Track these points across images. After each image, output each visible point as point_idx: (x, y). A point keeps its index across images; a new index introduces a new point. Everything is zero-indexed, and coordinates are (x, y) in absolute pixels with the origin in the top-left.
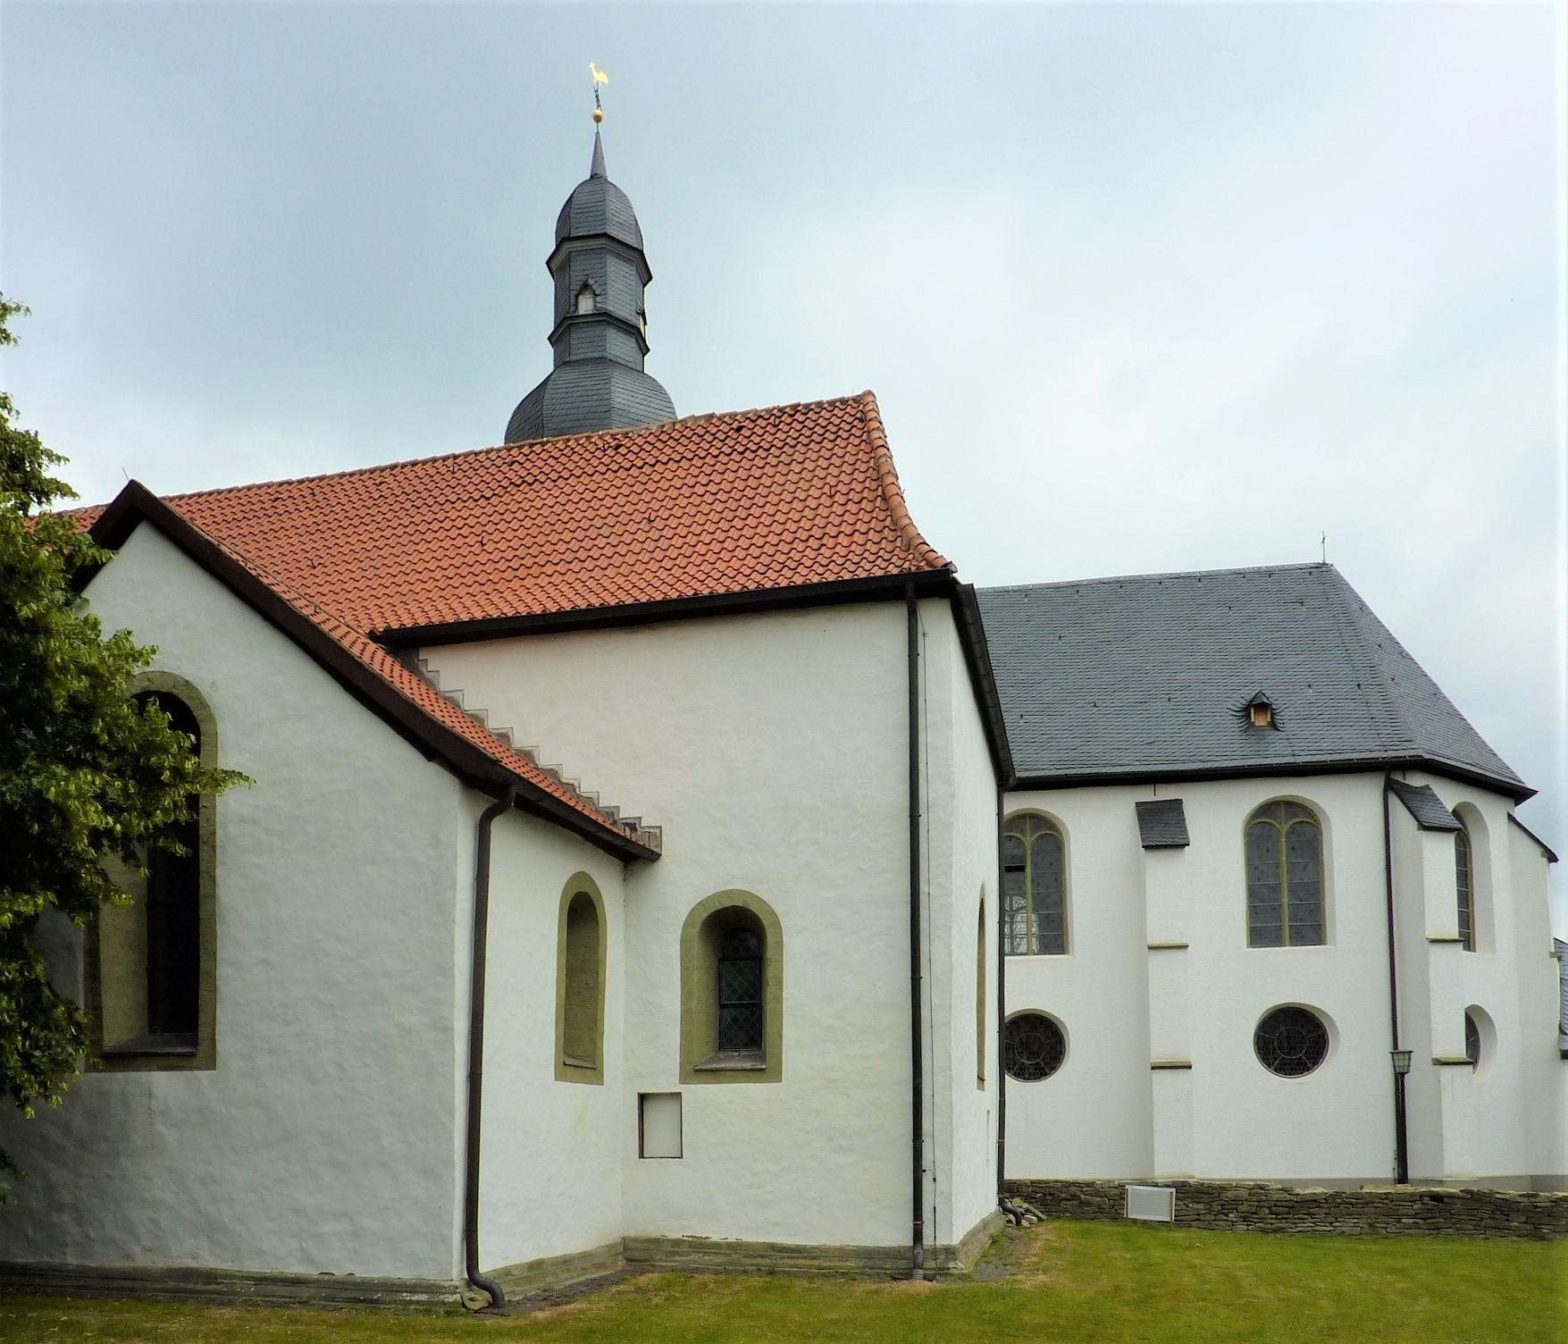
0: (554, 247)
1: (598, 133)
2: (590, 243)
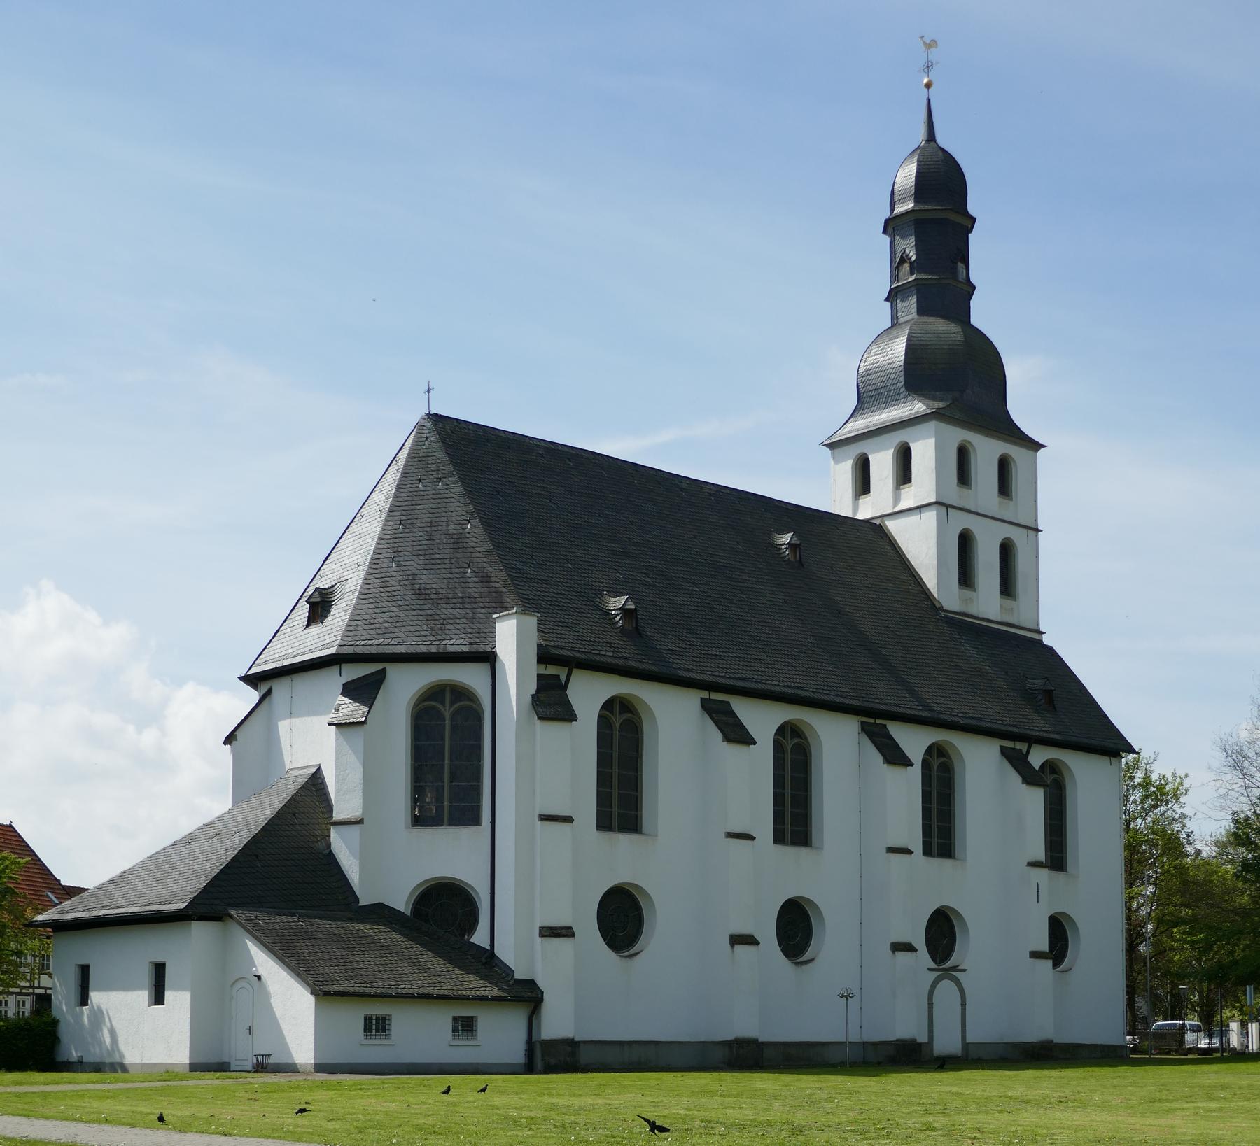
1: (929, 100)
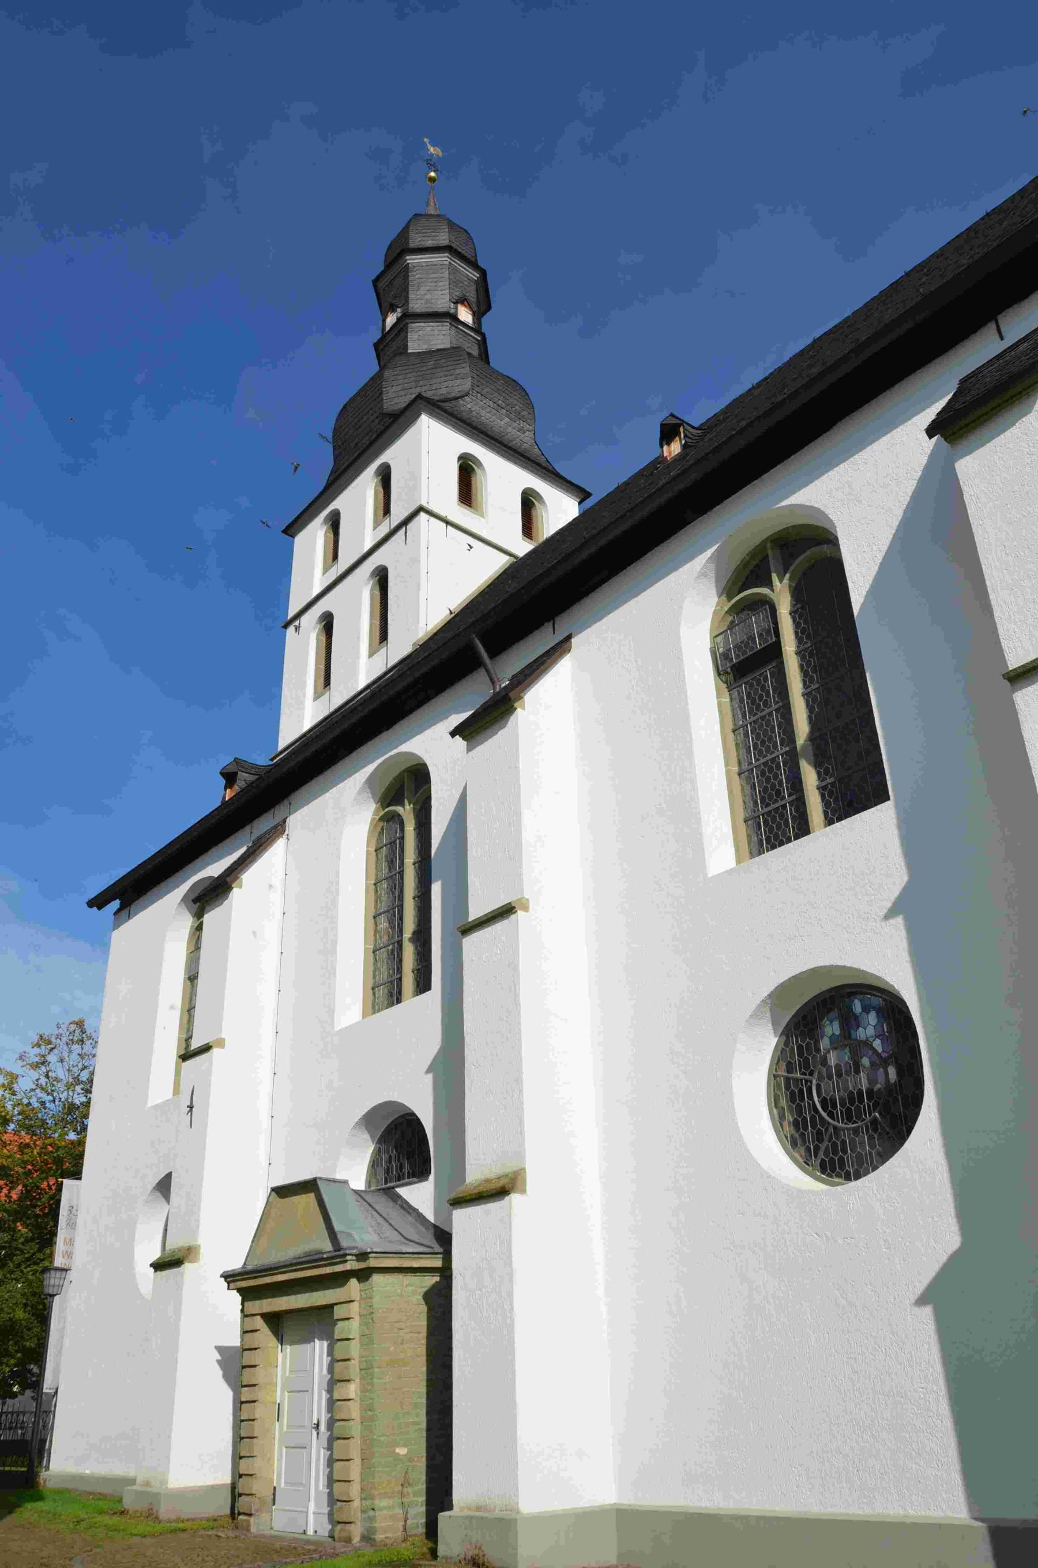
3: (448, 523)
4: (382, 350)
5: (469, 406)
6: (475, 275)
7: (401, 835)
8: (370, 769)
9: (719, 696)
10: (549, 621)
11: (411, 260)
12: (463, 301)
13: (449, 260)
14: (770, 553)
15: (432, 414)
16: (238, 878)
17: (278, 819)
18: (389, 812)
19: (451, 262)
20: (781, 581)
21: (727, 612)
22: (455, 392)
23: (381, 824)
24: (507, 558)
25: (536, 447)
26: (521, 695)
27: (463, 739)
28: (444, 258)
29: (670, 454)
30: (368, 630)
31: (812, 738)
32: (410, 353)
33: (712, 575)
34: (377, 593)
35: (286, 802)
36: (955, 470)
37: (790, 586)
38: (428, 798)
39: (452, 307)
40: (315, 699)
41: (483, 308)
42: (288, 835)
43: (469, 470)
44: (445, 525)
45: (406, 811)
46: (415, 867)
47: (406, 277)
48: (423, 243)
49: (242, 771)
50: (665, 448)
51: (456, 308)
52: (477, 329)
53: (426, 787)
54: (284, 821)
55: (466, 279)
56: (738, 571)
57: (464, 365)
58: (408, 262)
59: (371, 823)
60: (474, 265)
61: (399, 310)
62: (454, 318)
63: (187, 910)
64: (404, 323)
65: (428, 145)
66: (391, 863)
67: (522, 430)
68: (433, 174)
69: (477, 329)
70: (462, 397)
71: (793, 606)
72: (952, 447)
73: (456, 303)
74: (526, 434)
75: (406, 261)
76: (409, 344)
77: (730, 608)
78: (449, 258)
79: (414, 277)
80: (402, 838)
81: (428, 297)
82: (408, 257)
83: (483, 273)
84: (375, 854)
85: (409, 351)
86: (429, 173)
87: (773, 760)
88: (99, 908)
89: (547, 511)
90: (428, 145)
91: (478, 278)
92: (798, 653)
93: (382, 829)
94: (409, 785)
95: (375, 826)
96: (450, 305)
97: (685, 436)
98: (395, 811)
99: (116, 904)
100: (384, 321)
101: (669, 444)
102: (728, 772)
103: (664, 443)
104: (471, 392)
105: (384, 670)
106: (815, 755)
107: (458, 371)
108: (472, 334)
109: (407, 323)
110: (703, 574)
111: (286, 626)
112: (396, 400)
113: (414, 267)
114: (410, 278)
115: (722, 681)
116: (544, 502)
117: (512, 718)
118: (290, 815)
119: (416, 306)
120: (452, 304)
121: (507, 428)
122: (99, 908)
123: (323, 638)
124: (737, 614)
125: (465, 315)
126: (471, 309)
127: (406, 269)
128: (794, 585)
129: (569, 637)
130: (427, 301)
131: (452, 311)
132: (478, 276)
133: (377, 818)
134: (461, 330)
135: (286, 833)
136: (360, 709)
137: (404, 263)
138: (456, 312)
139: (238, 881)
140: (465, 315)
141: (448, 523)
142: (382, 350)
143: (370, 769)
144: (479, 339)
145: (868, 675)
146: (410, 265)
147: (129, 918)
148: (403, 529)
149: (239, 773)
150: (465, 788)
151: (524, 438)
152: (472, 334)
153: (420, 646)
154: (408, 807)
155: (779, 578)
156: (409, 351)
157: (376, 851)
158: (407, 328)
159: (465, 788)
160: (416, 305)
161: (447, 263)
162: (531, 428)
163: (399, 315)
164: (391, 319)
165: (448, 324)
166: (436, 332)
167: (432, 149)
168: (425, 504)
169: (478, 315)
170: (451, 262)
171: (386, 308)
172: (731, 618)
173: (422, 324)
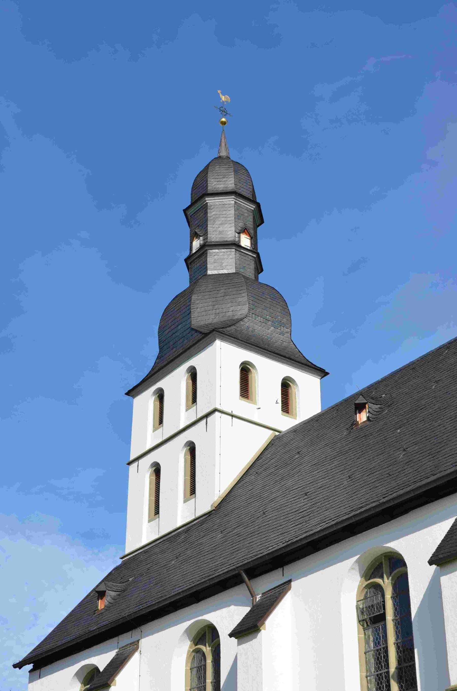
0: (190, 204)
2: (192, 210)
3: (233, 416)
4: (190, 263)
5: (247, 325)
6: (252, 207)
7: (204, 663)
8: (187, 624)
9: (359, 634)
10: (280, 567)
11: (210, 201)
12: (244, 230)
13: (235, 200)
14: (383, 561)
15: (223, 339)
16: (114, 680)
17: (134, 639)
18: (198, 648)
19: (236, 201)
20: (388, 579)
21: (364, 587)
22: (238, 315)
23: (194, 654)
24: (271, 432)
25: (292, 343)
26: (264, 622)
27: (235, 638)
28: (230, 200)
29: (361, 419)
30: (184, 466)
31: (399, 669)
32: (210, 275)
33: (357, 568)
34: (189, 457)
35: (138, 630)
36: (440, 580)
37: (392, 583)
38: (219, 645)
39: (237, 236)
40: (185, 502)
41: (258, 222)
42: (140, 651)
43: (247, 370)
44: (231, 417)
45: (207, 650)
46: (212, 685)
47: (206, 213)
48: (218, 186)
49: (108, 590)
50: (358, 415)
51: (239, 237)
52: (254, 249)
53: (217, 640)
54: (138, 641)
55: (246, 211)
56: (369, 568)
57: (243, 295)
58: (207, 202)
59: (188, 654)
60: (253, 200)
61: (201, 238)
62: (236, 245)
63: (77, 680)
64: (205, 249)
65: (220, 94)
66: (199, 678)
67: (282, 333)
68: (224, 120)
69: (254, 249)
70: (241, 320)
71: (393, 594)
72: (440, 569)
73: (239, 233)
74: (285, 336)
75: (206, 201)
76: (208, 266)
77: (366, 586)
78: (234, 199)
79: (211, 214)
80: (205, 665)
81: (221, 229)
82: (206, 199)
83: (258, 205)
84: (190, 671)
85: (209, 272)
86: (221, 119)
87: (381, 674)
88: (20, 668)
89: (298, 390)
90: (220, 94)
91: (254, 208)
92: (393, 620)
93: (194, 657)
94: (208, 637)
95: (190, 655)
96: (235, 235)
97: (369, 412)
98: (200, 649)
99: (30, 666)
100: (191, 243)
101: (360, 413)
102: (361, 676)
103: (357, 411)
104: (248, 315)
105: (193, 518)
106: (398, 679)
107: (240, 299)
108: (250, 254)
109: (207, 250)
110: (352, 568)
111: (130, 463)
112: (199, 319)
113: (211, 206)
114: (209, 215)
115: (361, 624)
116: (296, 384)
117: (259, 635)
118: (141, 639)
119: (213, 236)
120: (237, 234)
121: (273, 334)
122: (20, 668)
123: (154, 478)
124: (369, 589)
125: (245, 241)
126: (250, 236)
127: (205, 208)
128: (393, 582)
129: (290, 581)
130: (221, 232)
131: (237, 239)
132: (254, 207)
133: (191, 650)
134: (242, 252)
135: (139, 650)
136: (181, 593)
137: (204, 202)
138: (239, 241)
139: (113, 682)
140: (245, 241)
141: (233, 416)
142: (190, 263)
143: (187, 624)
144: (255, 256)
145: (416, 651)
146: (208, 204)
147: (40, 678)
148: (205, 420)
149: (107, 591)
150: (237, 654)
151: (283, 338)
152: (250, 254)
153: (216, 507)
154: (209, 649)
155: (387, 578)
156: (209, 272)
157: (191, 669)
158: (207, 254)
159: (237, 654)
160: (213, 237)
161: (233, 202)
162: (289, 330)
163: (202, 242)
164: (196, 244)
165: (234, 250)
166: (226, 256)
167: (223, 98)
168: (218, 407)
169: (254, 239)
170: (236, 201)
171: (194, 235)
172: (366, 590)
173: (217, 250)
